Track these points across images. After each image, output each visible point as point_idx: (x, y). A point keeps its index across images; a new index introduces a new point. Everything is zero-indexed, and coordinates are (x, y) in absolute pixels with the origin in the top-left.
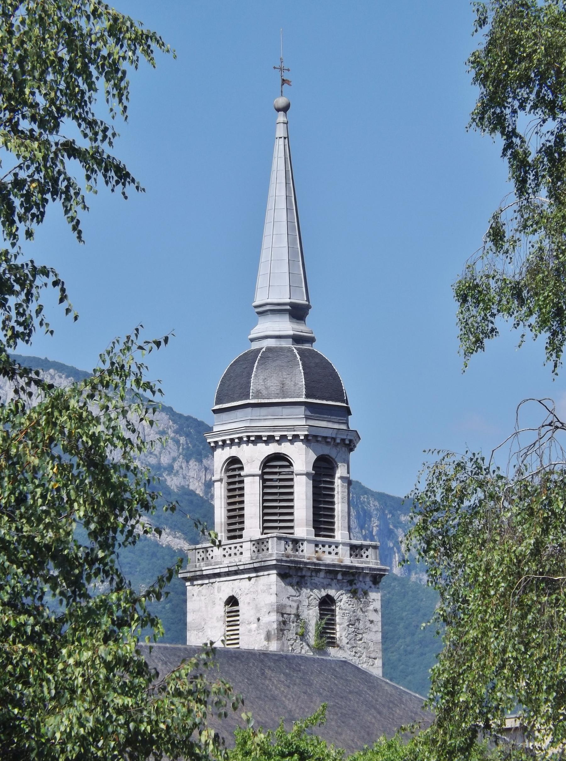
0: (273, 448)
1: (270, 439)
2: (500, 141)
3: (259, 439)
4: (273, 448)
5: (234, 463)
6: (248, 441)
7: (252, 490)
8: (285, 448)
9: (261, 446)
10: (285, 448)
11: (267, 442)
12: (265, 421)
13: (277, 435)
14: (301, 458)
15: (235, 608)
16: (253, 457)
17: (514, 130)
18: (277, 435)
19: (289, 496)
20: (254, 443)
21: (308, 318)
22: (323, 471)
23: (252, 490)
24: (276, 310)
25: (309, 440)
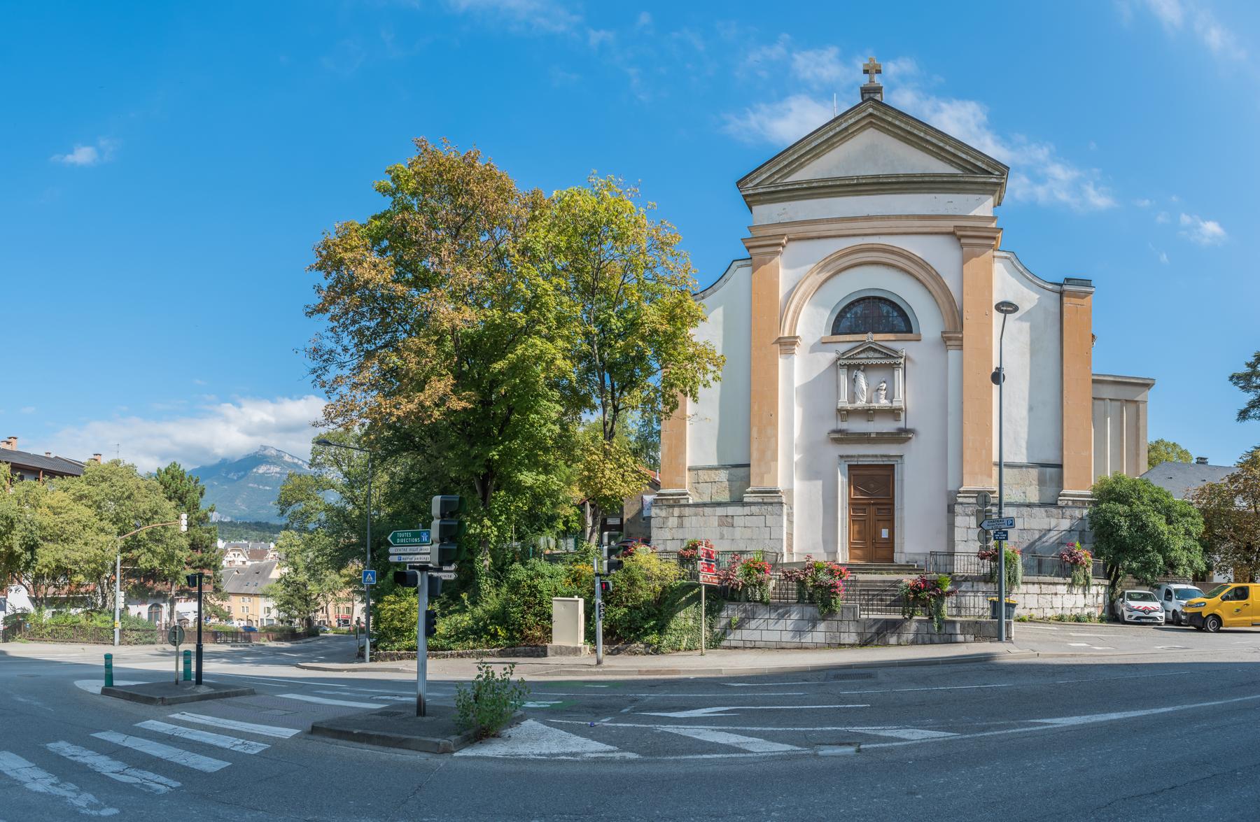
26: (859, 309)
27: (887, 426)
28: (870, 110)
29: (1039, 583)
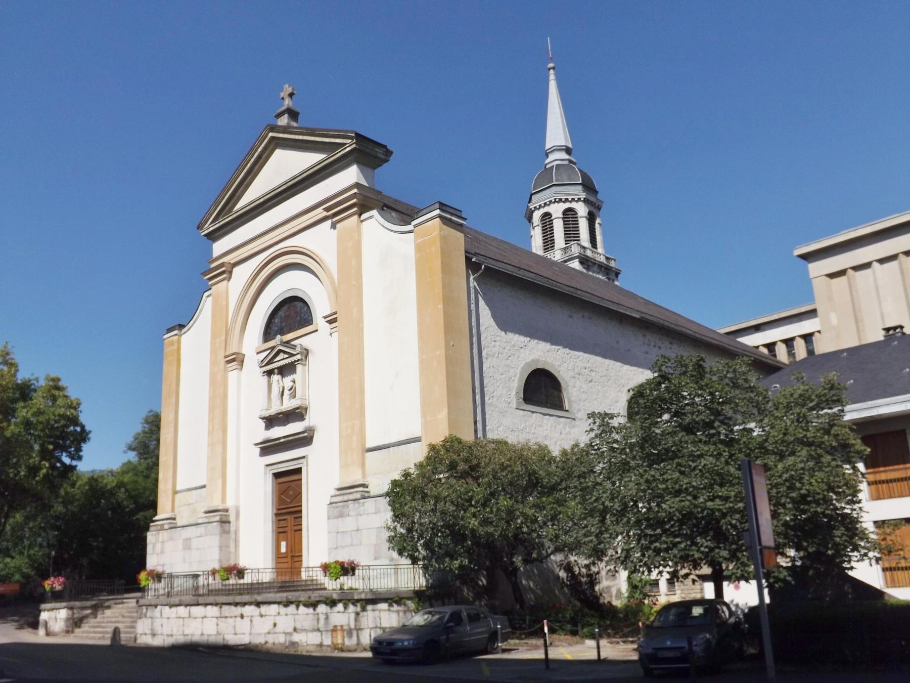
0: (567, 205)
1: (567, 200)
2: (306, 628)
3: (560, 200)
4: (567, 205)
5: (547, 215)
6: (555, 201)
7: (558, 227)
8: (573, 205)
9: (561, 204)
10: (573, 205)
11: (564, 202)
12: (562, 192)
13: (570, 198)
14: (582, 210)
15: (339, 628)
16: (557, 210)
17: (317, 645)
18: (570, 198)
19: (576, 229)
20: (558, 202)
21: (307, 417)
22: (591, 218)
23: (558, 227)
24: (559, 149)
25: (586, 201)
26: (281, 313)
27: (294, 428)
28: (271, 134)
29: (216, 605)
